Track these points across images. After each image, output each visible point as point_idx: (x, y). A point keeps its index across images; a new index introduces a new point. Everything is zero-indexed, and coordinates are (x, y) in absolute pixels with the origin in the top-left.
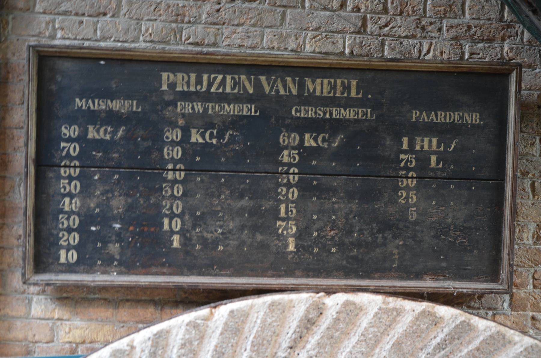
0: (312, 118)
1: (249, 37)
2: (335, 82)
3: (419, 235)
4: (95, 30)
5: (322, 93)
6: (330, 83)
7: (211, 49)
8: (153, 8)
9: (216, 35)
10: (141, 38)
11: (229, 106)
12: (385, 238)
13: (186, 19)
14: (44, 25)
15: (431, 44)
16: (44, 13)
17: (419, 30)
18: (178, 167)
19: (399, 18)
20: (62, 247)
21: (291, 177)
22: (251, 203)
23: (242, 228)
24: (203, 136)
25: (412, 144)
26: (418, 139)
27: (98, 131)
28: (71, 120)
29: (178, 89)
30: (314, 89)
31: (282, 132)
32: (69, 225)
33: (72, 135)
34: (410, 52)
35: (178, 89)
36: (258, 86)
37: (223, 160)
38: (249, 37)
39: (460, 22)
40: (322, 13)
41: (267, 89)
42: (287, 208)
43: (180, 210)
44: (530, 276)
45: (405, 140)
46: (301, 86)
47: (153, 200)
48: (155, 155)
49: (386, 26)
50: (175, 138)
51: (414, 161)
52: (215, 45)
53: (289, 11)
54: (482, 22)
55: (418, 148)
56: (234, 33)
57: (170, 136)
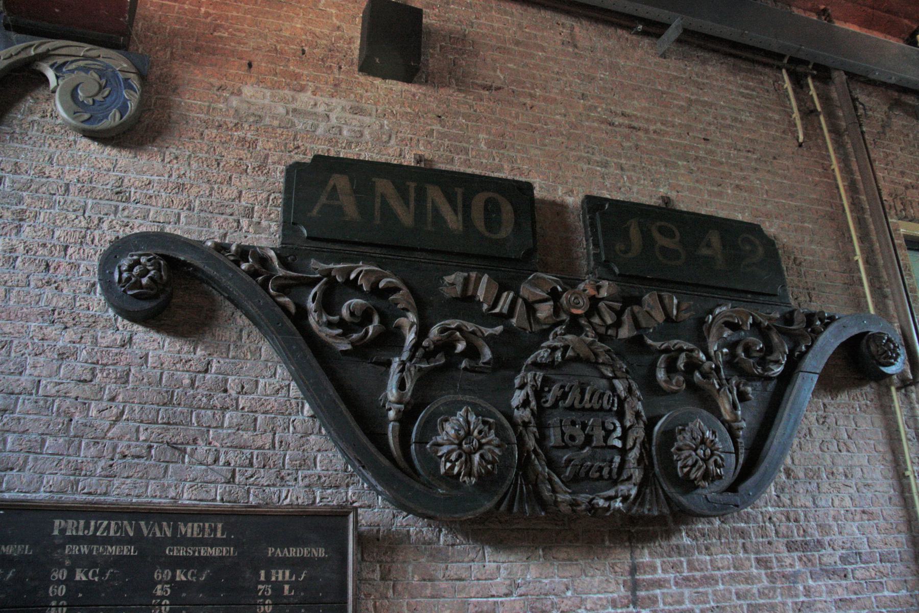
0: (183, 556)
1: (135, 487)
2: (204, 525)
5: (192, 534)
6: (199, 526)
7: (102, 498)
8: (55, 463)
9: (107, 487)
10: (42, 489)
11: (112, 547)
13: (83, 473)
17: (278, 480)
18: (61, 603)
19: (262, 470)
24: (86, 575)
25: (268, 576)
26: (273, 571)
29: (67, 534)
30: (186, 532)
31: (157, 569)
35: (67, 534)
36: (138, 530)
38: (135, 487)
39: (313, 472)
40: (199, 467)
41: (145, 532)
45: (263, 573)
46: (175, 529)
49: (252, 477)
50: (61, 577)
51: (270, 590)
52: (105, 494)
53: (171, 465)
54: (330, 473)
55: (273, 579)
56: (123, 484)
57: (56, 576)
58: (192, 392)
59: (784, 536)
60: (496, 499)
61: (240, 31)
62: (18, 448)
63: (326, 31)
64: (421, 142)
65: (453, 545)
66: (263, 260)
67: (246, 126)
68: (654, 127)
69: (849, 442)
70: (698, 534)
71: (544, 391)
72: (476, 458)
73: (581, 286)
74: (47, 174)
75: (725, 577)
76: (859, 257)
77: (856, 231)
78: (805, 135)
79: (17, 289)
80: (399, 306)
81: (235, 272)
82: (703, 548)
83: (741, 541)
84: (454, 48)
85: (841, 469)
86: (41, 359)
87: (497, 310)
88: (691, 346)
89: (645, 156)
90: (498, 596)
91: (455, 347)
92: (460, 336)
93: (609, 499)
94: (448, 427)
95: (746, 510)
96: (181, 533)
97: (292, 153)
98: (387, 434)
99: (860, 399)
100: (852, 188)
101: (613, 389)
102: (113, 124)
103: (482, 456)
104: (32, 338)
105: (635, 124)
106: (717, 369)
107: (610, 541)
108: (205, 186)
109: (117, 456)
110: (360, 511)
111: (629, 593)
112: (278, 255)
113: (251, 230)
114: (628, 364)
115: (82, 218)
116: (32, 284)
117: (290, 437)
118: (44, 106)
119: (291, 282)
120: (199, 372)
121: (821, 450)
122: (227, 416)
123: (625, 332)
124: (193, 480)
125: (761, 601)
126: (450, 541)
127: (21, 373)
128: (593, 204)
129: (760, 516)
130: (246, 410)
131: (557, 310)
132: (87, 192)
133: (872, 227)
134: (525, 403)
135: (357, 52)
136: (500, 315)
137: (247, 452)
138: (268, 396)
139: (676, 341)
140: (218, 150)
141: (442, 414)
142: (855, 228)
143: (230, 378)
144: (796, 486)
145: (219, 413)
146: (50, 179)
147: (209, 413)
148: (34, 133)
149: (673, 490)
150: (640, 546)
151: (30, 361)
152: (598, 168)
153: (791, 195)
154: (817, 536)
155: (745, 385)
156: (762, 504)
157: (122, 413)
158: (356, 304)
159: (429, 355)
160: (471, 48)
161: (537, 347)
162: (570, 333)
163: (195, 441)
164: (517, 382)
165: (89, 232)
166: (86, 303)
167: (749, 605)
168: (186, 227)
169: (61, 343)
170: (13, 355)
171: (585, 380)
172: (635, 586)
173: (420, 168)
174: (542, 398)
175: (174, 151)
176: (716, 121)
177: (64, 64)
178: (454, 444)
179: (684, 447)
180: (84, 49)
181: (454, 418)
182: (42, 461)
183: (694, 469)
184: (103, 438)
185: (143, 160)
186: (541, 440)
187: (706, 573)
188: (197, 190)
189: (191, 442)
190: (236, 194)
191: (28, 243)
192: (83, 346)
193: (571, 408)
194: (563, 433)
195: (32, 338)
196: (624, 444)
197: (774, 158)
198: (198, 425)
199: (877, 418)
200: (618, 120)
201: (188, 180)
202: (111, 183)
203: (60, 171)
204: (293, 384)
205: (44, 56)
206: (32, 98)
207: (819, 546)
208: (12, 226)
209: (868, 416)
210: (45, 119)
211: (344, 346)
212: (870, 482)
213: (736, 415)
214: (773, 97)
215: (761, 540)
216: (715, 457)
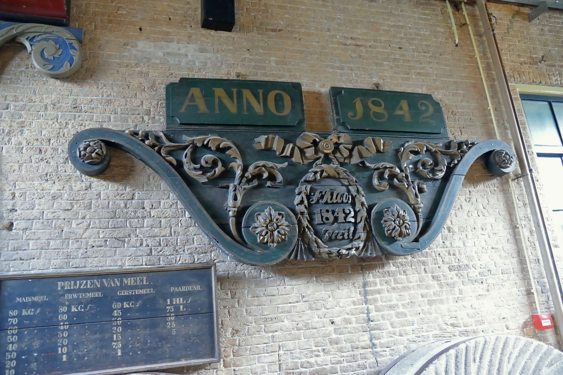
0: (127, 295)
2: (137, 279)
3: (177, 341)
4: (29, 266)
5: (131, 284)
6: (134, 279)
10: (51, 267)
11: (89, 293)
12: (162, 344)
14: (4, 266)
15: (180, 257)
16: (5, 261)
19: (166, 247)
20: (7, 369)
21: (118, 322)
22: (100, 336)
23: (96, 348)
24: (77, 308)
25: (171, 302)
26: (174, 299)
27: (27, 312)
28: (14, 308)
32: (11, 357)
33: (14, 315)
34: (171, 261)
36: (102, 283)
37: (87, 318)
39: (193, 246)
41: (106, 285)
42: (117, 336)
43: (66, 343)
44: (231, 351)
45: (169, 300)
46: (122, 282)
47: (53, 340)
48: (55, 319)
49: (161, 251)
51: (173, 309)
53: (118, 249)
55: (174, 303)
58: (126, 210)
59: (447, 263)
60: (288, 253)
61: (132, 9)
62: (36, 247)
63: (182, 6)
64: (239, 65)
65: (268, 278)
66: (157, 138)
67: (142, 64)
68: (370, 44)
69: (484, 211)
70: (399, 265)
71: (311, 195)
72: (276, 233)
73: (330, 137)
74: (34, 101)
75: (415, 286)
76: (491, 107)
77: (489, 93)
78: (459, 39)
79: (25, 164)
80: (231, 157)
81: (142, 146)
82: (402, 272)
83: (423, 267)
84: (254, 9)
85: (479, 226)
86: (43, 200)
87: (284, 154)
88: (391, 165)
89: (365, 61)
90: (293, 303)
91: (262, 176)
92: (265, 170)
93: (349, 249)
94: (260, 218)
95: (425, 250)
96: (125, 283)
97: (169, 78)
98: (229, 224)
99: (491, 186)
100: (488, 68)
101: (349, 191)
102: (66, 70)
103: (279, 232)
104: (37, 190)
105: (359, 43)
106: (407, 177)
107: (351, 270)
108: (123, 100)
109: (89, 247)
110: (217, 264)
111: (363, 297)
112: (164, 134)
113: (150, 122)
114: (357, 177)
115: (56, 123)
116: (33, 161)
117: (179, 229)
118: (27, 62)
119: (174, 148)
120: (129, 200)
121: (468, 216)
122: (146, 221)
123: (355, 160)
124: (130, 256)
125: (435, 298)
126: (266, 276)
127: (33, 209)
128: (336, 92)
129: (433, 253)
130: (155, 217)
131: (316, 152)
132: (58, 109)
133: (499, 89)
134: (302, 202)
135: (200, 16)
136: (286, 157)
137: (157, 239)
138: (166, 209)
139: (383, 163)
140: (127, 80)
141: (257, 211)
142: (488, 91)
143: (146, 201)
144: (453, 236)
145: (141, 220)
146: (35, 103)
147: (136, 220)
148: (23, 77)
149: (383, 243)
150: (368, 273)
151: (37, 201)
152: (338, 71)
153: (450, 75)
154: (466, 262)
155: (422, 184)
156: (435, 247)
157: (90, 224)
158: (208, 157)
159: (249, 181)
160: (264, 8)
161: (306, 172)
162: (324, 163)
163: (129, 235)
164: (297, 191)
165: (61, 130)
166: (64, 169)
167: (428, 300)
168: (115, 123)
169: (52, 191)
170: (27, 199)
171: (332, 188)
172: (366, 293)
173: (239, 80)
174: (310, 199)
175: (103, 82)
176: (406, 37)
177: (34, 37)
178: (263, 227)
179: (388, 220)
180: (44, 28)
181: (263, 213)
182: (49, 253)
183: (394, 231)
184: (81, 238)
185: (86, 88)
186: (311, 221)
187: (404, 285)
188: (118, 102)
189: (127, 236)
190: (140, 103)
191: (28, 139)
192: (65, 192)
193: (326, 203)
194: (322, 217)
195: (37, 190)
196: (356, 220)
197: (441, 55)
198: (131, 227)
199: (500, 196)
200: (349, 42)
201: (113, 97)
202: (70, 103)
203: (41, 98)
204: (179, 201)
205: (22, 34)
206: (19, 58)
207: (467, 267)
208: (18, 131)
209: (496, 196)
210: (28, 69)
211: (204, 180)
212: (496, 232)
213: (417, 201)
214: (440, 18)
215: (434, 266)
216: (405, 224)
